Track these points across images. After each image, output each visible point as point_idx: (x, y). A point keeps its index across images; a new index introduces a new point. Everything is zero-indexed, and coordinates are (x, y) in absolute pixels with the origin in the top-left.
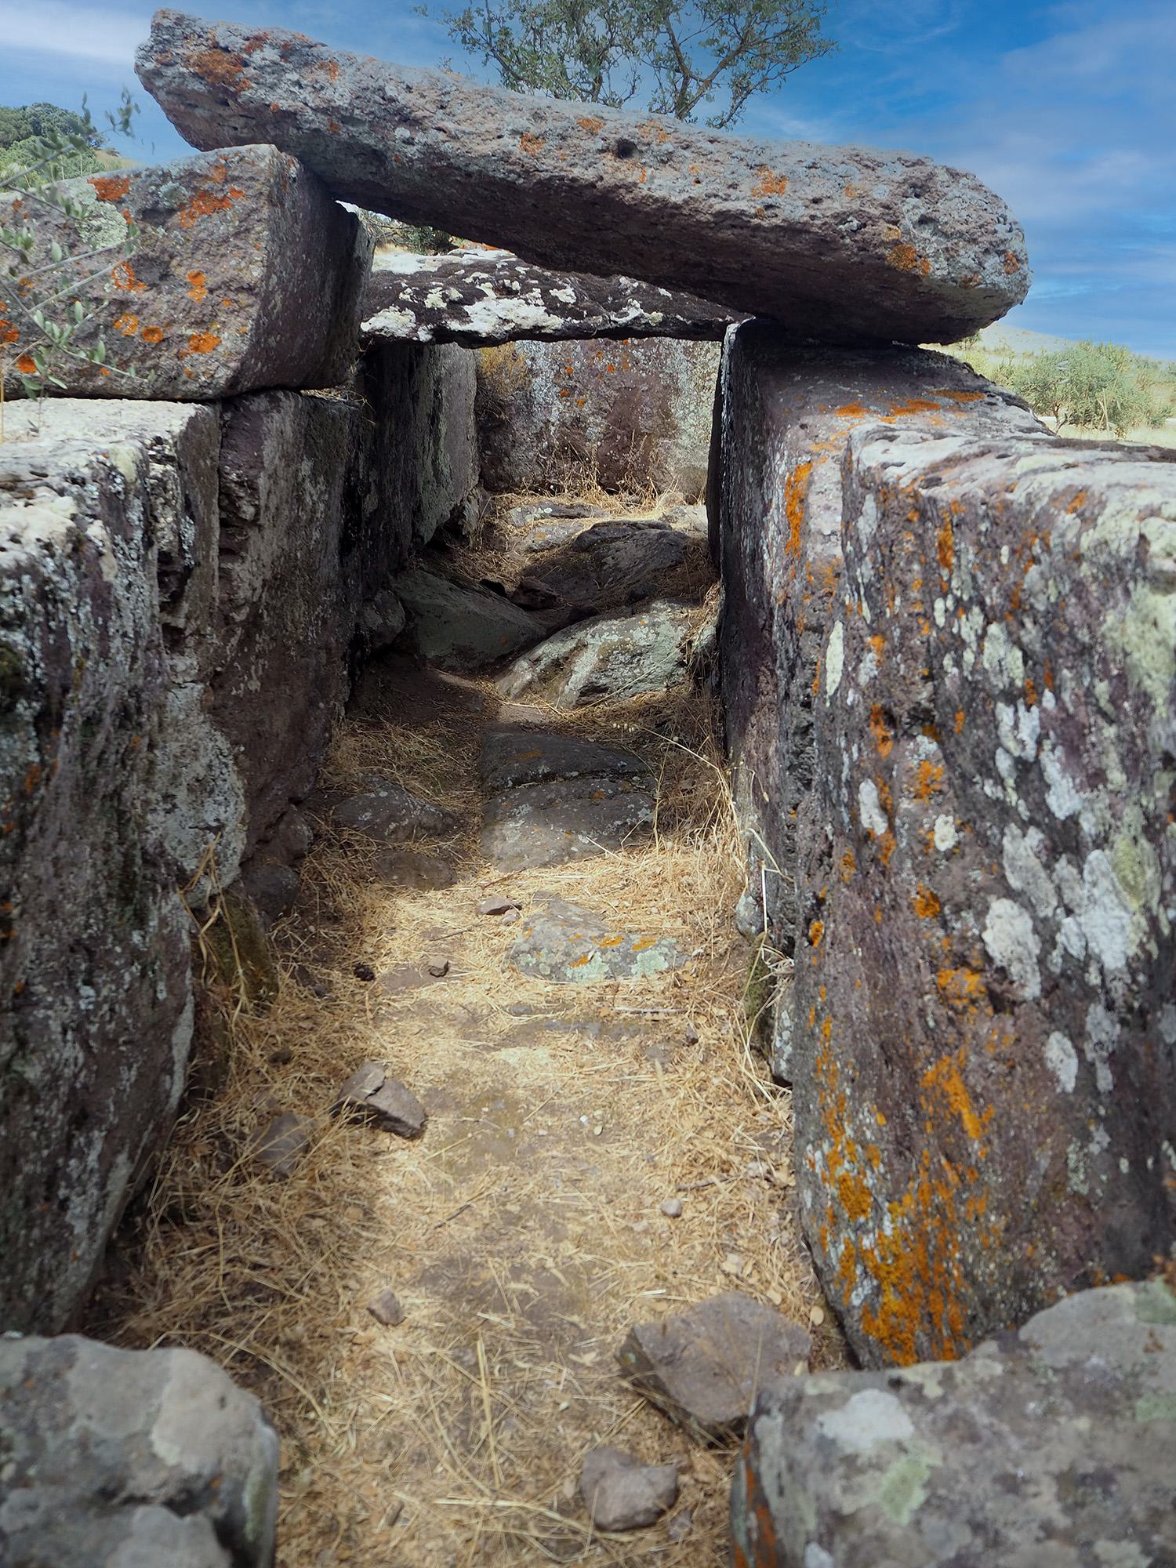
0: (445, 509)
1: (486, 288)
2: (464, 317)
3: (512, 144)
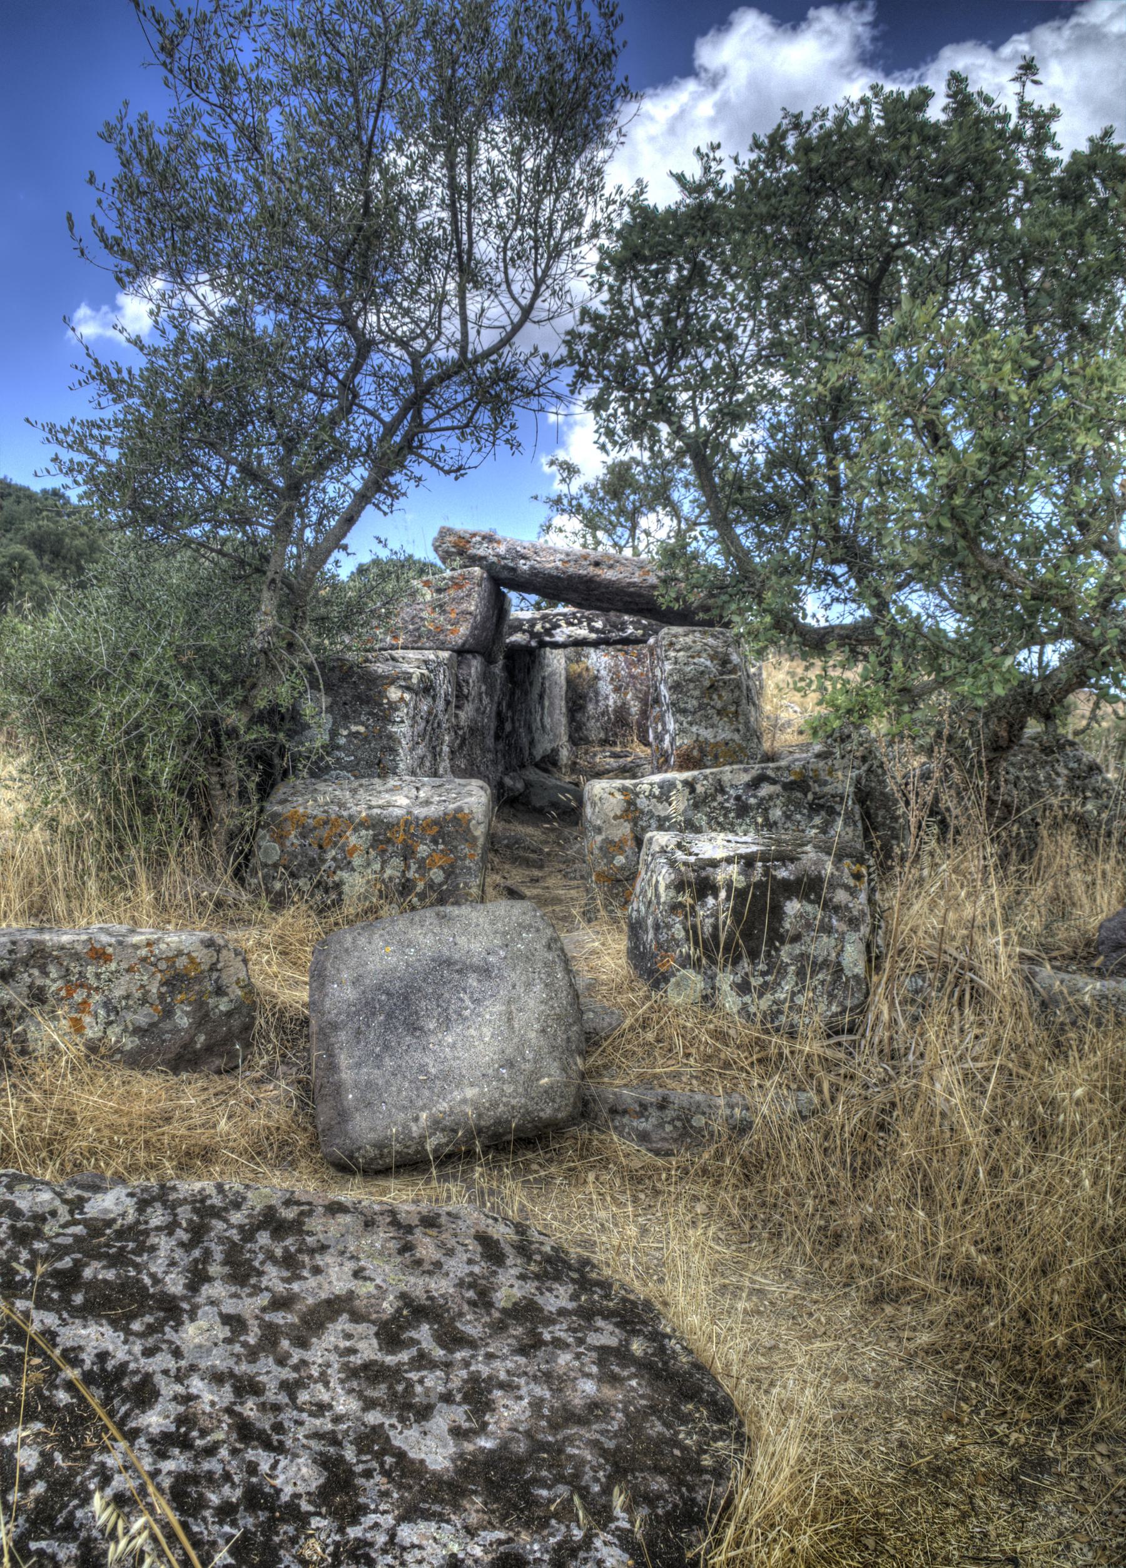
0: (549, 747)
1: (562, 623)
2: (552, 636)
3: (559, 564)
